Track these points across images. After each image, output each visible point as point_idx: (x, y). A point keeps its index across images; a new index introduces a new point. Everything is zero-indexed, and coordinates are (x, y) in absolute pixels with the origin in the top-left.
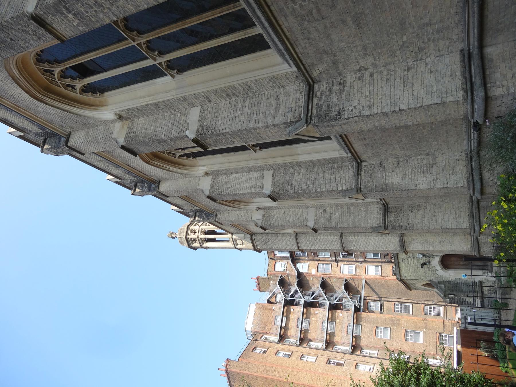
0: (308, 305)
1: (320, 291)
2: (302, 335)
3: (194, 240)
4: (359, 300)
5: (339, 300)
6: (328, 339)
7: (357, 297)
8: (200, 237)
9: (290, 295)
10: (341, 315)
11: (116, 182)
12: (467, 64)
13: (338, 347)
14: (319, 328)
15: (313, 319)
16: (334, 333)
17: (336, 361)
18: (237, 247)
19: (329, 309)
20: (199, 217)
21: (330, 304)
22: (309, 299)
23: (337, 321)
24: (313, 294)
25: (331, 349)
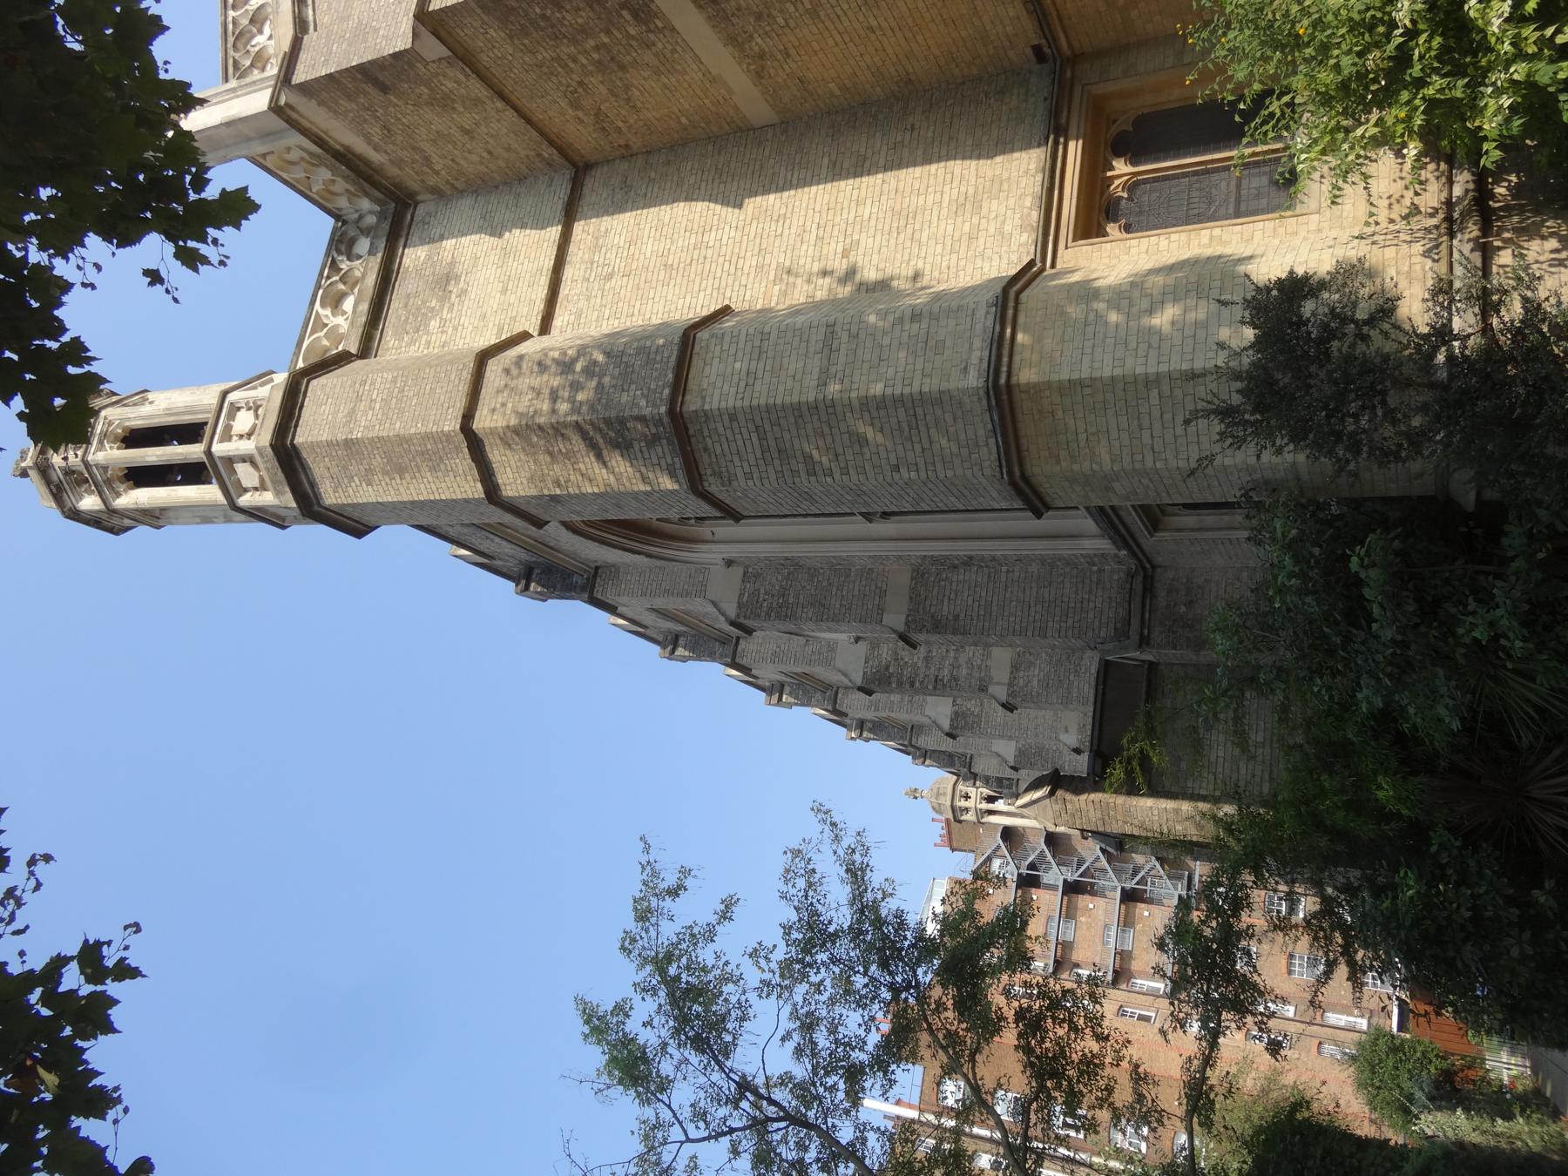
0: (1072, 889)
1: (1098, 858)
2: (1059, 954)
3: (967, 810)
4: (1185, 882)
5: (1143, 881)
6: (1117, 965)
7: (1183, 875)
8: (979, 806)
9: (1027, 863)
10: (1146, 914)
11: (476, 564)
12: (1163, 241)
13: (1139, 981)
14: (1098, 941)
15: (1083, 919)
16: (1131, 952)
17: (1138, 1012)
18: (245, 500)
19: (1122, 901)
20: (790, 694)
21: (1123, 889)
22: (1072, 876)
23: (1139, 927)
24: (1080, 864)
25: (1124, 986)
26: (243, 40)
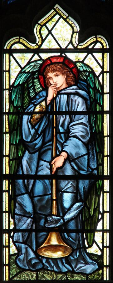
26: (64, 239)
